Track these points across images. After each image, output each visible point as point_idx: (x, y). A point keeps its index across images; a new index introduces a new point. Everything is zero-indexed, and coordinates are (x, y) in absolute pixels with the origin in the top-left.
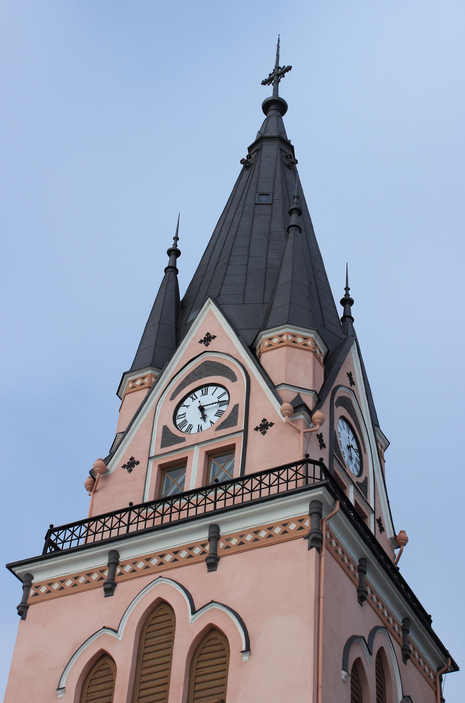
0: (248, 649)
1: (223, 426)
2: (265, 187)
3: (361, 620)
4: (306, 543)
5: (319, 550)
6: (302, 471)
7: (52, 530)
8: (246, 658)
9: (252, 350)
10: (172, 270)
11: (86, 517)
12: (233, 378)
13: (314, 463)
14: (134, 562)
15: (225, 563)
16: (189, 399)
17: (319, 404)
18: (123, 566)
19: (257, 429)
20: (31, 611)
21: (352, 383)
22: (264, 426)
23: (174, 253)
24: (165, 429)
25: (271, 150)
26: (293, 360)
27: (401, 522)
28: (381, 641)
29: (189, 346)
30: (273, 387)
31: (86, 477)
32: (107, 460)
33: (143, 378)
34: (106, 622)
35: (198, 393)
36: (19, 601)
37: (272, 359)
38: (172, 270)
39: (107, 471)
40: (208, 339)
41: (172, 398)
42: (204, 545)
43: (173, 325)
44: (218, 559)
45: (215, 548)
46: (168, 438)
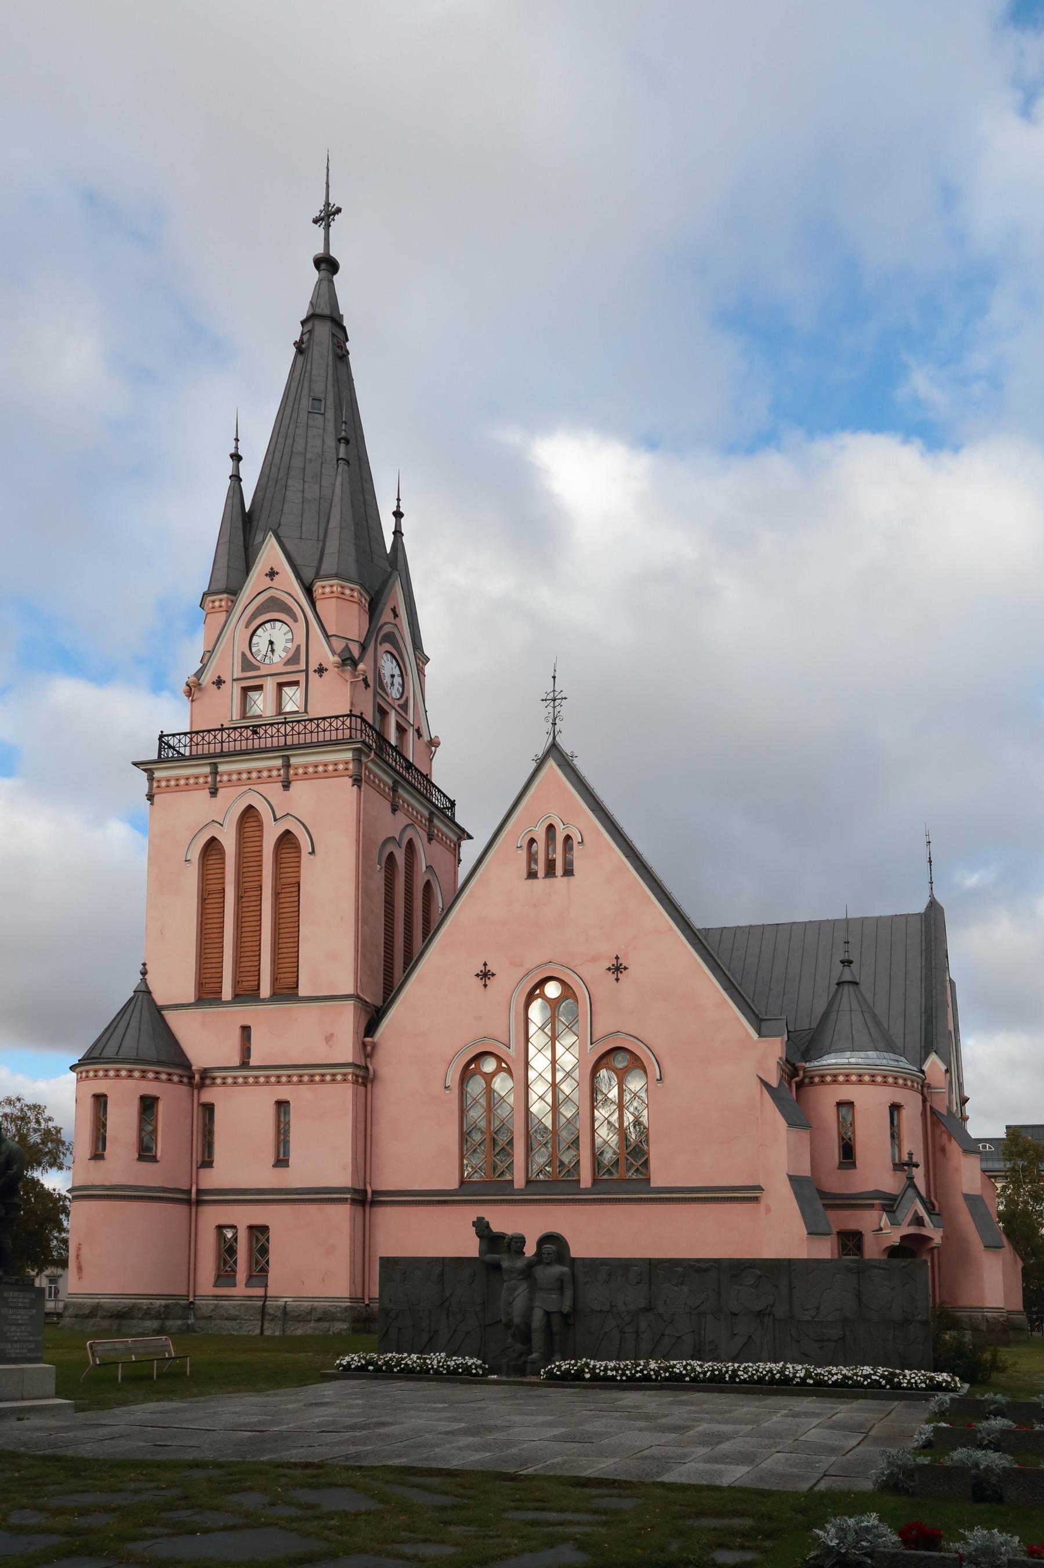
0: (313, 852)
1: (288, 662)
2: (318, 389)
3: (391, 825)
4: (350, 781)
5: (359, 787)
6: (348, 723)
7: (161, 737)
8: (312, 857)
9: (308, 591)
10: (236, 478)
11: (188, 730)
12: (296, 620)
13: (356, 716)
14: (230, 774)
15: (294, 786)
16: (260, 630)
17: (363, 648)
18: (221, 776)
19: (315, 671)
20: (156, 798)
21: (396, 615)
22: (321, 670)
23: (236, 457)
24: (243, 654)
25: (323, 330)
26: (342, 613)
27: (436, 728)
28: (410, 833)
29: (256, 579)
30: (327, 637)
31: (184, 687)
32: (199, 674)
33: (221, 600)
34: (215, 814)
35: (268, 625)
36: (146, 791)
37: (328, 608)
38: (236, 478)
39: (200, 684)
40: (272, 574)
41: (247, 626)
42: (279, 770)
43: (242, 544)
44: (290, 783)
45: (287, 773)
46: (247, 665)
